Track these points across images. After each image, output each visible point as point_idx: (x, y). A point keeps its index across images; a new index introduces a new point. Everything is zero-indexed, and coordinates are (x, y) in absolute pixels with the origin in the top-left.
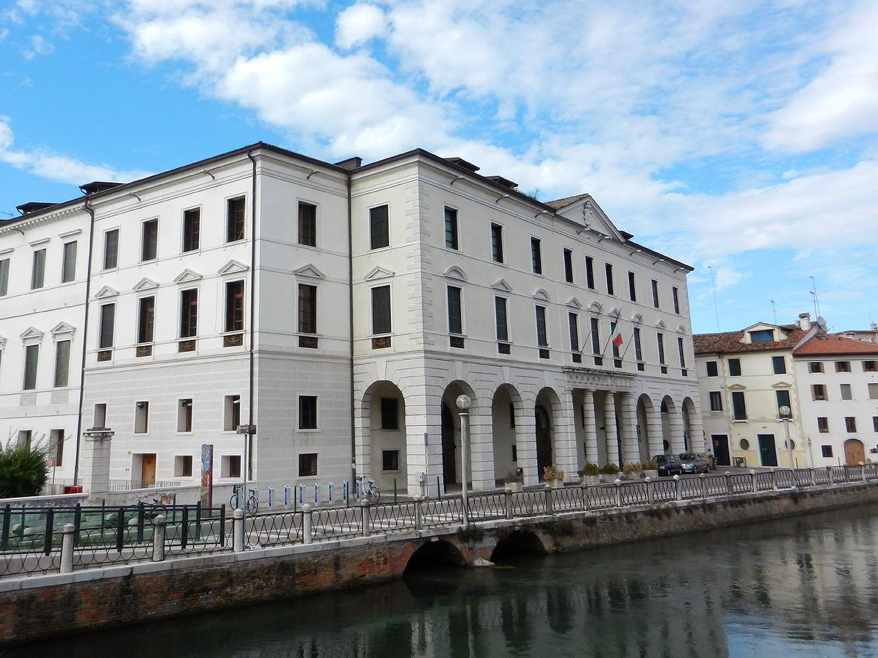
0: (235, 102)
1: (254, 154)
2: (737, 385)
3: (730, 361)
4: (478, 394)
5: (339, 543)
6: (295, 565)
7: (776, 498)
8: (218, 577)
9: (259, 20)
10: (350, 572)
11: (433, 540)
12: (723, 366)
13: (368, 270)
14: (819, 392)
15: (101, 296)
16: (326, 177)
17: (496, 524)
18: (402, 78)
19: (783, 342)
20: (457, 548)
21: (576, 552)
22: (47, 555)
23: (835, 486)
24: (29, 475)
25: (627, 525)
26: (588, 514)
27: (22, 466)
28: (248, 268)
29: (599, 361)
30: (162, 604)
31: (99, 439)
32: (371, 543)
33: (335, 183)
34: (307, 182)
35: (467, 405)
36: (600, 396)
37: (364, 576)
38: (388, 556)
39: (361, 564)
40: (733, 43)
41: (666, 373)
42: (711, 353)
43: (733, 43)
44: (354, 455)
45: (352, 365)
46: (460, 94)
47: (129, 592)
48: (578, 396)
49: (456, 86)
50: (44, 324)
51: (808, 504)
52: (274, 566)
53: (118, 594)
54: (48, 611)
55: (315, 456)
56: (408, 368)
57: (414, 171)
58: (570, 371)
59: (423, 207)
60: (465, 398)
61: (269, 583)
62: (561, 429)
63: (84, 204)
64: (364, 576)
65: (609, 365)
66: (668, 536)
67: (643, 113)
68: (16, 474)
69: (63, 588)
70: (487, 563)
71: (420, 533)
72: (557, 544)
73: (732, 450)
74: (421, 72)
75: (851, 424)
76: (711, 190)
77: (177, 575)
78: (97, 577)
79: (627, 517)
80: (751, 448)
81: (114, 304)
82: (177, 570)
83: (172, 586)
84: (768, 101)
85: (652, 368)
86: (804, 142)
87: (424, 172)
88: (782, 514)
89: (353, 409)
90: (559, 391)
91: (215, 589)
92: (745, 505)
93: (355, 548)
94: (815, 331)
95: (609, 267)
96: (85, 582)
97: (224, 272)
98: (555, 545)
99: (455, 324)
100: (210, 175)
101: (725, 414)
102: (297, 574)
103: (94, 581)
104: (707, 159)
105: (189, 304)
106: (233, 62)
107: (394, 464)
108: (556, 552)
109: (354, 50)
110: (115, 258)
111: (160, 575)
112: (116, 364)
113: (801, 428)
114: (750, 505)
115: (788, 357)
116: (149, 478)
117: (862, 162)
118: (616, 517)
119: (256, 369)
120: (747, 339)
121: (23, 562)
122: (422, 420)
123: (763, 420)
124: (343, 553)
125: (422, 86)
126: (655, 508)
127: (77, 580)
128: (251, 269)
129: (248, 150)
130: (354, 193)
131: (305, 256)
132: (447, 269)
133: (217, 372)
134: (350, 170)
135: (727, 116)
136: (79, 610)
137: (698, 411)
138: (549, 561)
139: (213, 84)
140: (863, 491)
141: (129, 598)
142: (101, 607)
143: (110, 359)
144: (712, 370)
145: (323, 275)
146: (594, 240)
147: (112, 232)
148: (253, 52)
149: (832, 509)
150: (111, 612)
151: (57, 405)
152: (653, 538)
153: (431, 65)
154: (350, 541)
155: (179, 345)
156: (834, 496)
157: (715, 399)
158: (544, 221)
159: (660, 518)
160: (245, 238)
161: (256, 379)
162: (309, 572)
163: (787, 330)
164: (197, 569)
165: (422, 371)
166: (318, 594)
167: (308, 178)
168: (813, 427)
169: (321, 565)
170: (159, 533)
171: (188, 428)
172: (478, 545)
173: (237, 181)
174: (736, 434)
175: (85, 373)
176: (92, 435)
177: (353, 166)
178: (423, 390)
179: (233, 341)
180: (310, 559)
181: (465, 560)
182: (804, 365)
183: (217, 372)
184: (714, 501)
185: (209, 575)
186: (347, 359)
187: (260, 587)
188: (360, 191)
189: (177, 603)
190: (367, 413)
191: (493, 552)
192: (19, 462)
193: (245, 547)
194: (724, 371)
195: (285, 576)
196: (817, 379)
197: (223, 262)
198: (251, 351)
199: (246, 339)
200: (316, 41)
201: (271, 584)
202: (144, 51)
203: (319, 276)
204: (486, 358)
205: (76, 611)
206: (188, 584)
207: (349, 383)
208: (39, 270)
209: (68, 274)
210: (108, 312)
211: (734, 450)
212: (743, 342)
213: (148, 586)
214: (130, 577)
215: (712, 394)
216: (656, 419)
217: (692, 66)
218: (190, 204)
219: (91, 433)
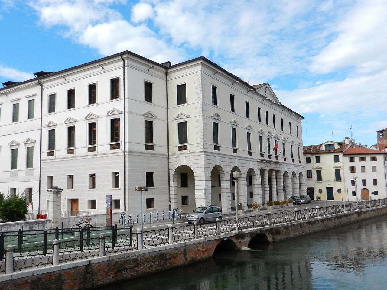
0: (88, 46)
1: (124, 57)
2: (318, 167)
3: (316, 157)
4: (242, 172)
5: (186, 243)
6: (166, 254)
7: (352, 214)
8: (131, 263)
9: (97, 8)
10: (191, 256)
11: (225, 239)
12: (313, 159)
13: (176, 115)
14: (352, 169)
15: (48, 126)
16: (156, 69)
17: (250, 230)
18: (161, 37)
19: (338, 149)
20: (234, 242)
21: (281, 241)
22: (45, 256)
23: (371, 208)
24: (19, 209)
25: (300, 228)
26: (286, 224)
27: (16, 205)
28: (122, 112)
29: (277, 158)
30: (105, 278)
31: (55, 193)
32: (199, 242)
33: (160, 73)
34: (148, 72)
35: (238, 176)
36: (270, 171)
37: (197, 257)
38: (206, 248)
39: (195, 252)
40: (299, 26)
41: (286, 161)
42: (308, 154)
43: (299, 26)
44: (170, 199)
45: (168, 158)
46: (186, 45)
47: (89, 273)
48: (262, 171)
49: (184, 41)
50: (20, 139)
51: (363, 216)
52: (157, 256)
53: (83, 274)
54: (48, 285)
55: (153, 199)
56: (195, 158)
57: (199, 67)
58: (260, 161)
59: (203, 84)
60: (237, 173)
61: (155, 264)
62: (256, 186)
63: (37, 81)
64: (197, 257)
65: (273, 159)
66: (315, 233)
67: (262, 56)
68: (13, 209)
69: (55, 273)
70: (248, 249)
71: (220, 236)
72: (274, 238)
73: (315, 194)
74: (169, 35)
75: (364, 182)
76: (287, 89)
77: (112, 263)
78: (73, 266)
79: (300, 225)
80: (323, 193)
81: (55, 129)
82: (112, 260)
83: (110, 268)
84: (312, 51)
85: (289, 161)
86: (326, 70)
87: (203, 67)
88: (354, 221)
89: (169, 178)
90: (255, 170)
91: (130, 268)
92: (341, 218)
93: (193, 245)
94: (351, 145)
95: (274, 116)
96: (66, 269)
97: (110, 114)
98: (273, 239)
99: (216, 140)
100: (101, 67)
101: (313, 179)
102: (168, 259)
103: (71, 268)
104: (287, 76)
105: (92, 129)
106: (86, 27)
107: (186, 202)
108: (273, 242)
109: (140, 24)
110: (54, 108)
111: (104, 264)
112: (57, 157)
113: (344, 184)
114: (343, 218)
115: (341, 155)
116: (75, 210)
117: (347, 78)
118: (296, 225)
119: (127, 160)
120: (323, 148)
121: (33, 260)
122: (203, 183)
123: (329, 181)
124: (187, 247)
125: (169, 41)
126: (310, 220)
127: (63, 268)
128: (123, 112)
129: (121, 54)
130: (169, 78)
131: (147, 107)
132: (213, 114)
133: (107, 161)
134: (167, 67)
135: (296, 58)
136: (65, 284)
137: (304, 178)
138: (270, 247)
139: (78, 37)
140: (380, 210)
141: (89, 276)
142: (75, 281)
143: (54, 155)
144: (308, 161)
145: (156, 117)
146: (269, 104)
147: (52, 95)
148: (95, 23)
149: (371, 218)
150: (80, 283)
151: (28, 176)
152: (309, 234)
153: (173, 31)
154: (190, 242)
155: (67, 151)
156: (371, 213)
157: (309, 173)
158: (250, 94)
159: (312, 225)
160: (120, 98)
161: (127, 164)
162: (173, 258)
163: (340, 144)
164: (122, 259)
165: (203, 161)
166: (177, 268)
167: (149, 70)
168: (349, 185)
169: (178, 254)
170: (102, 242)
171: (94, 187)
172: (243, 241)
173: (116, 70)
174: (317, 187)
175: (42, 162)
176: (52, 191)
177: (167, 66)
178: (203, 170)
179: (115, 146)
180: (173, 251)
181: (237, 247)
182: (347, 159)
183: (107, 161)
184: (331, 217)
185: (127, 262)
186: (166, 155)
187: (151, 266)
188: (172, 77)
189: (113, 276)
190: (175, 180)
191: (249, 243)
192: (14, 203)
193: (143, 247)
194: (313, 161)
195: (162, 260)
196: (352, 164)
197: (109, 110)
198: (124, 151)
199: (122, 146)
200: (122, 19)
201: (156, 264)
202: (45, 20)
203: (154, 117)
204: (228, 155)
205: (63, 284)
206: (117, 266)
207: (167, 166)
208: (16, 112)
209: (30, 115)
210: (51, 133)
211: (316, 194)
212: (322, 149)
213: (99, 269)
214: (89, 265)
215: (308, 171)
216: (289, 182)
217: (282, 35)
218: (91, 81)
219: (52, 190)
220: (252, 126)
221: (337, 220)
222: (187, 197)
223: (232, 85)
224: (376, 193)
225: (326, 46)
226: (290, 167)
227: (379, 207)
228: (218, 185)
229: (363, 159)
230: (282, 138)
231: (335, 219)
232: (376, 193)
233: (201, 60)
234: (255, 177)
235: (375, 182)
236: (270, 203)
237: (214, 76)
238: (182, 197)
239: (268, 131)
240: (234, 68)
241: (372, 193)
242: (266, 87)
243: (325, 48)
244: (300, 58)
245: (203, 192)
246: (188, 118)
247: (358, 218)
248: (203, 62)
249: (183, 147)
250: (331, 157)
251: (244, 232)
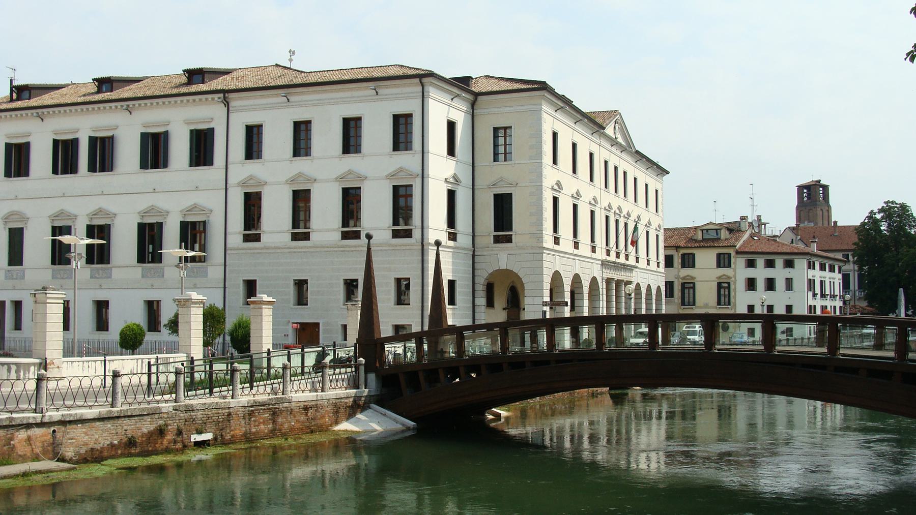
48: (609, 281)
58: (604, 264)
65: (622, 260)
95: (555, 135)
196: (751, 273)
199: (417, 234)
218: (351, 112)
223: (573, 125)
241: (783, 332)
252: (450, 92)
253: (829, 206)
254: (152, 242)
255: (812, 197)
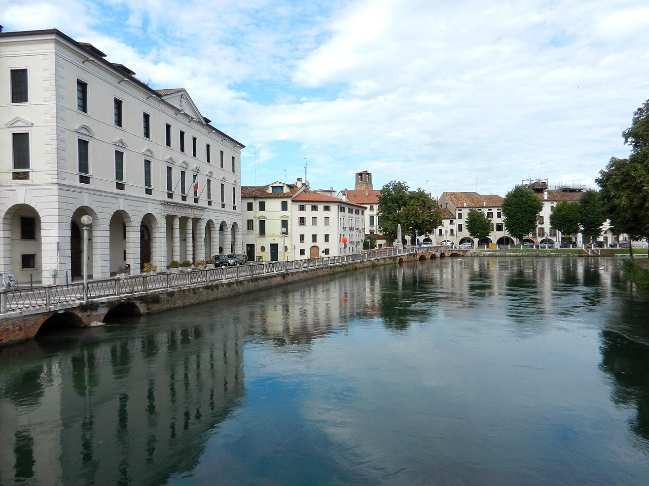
3: (283, 202)
4: (99, 216)
7: (275, 276)
12: (256, 205)
14: (302, 221)
23: (303, 269)
26: (170, 290)
36: (183, 220)
42: (250, 197)
48: (170, 219)
51: (289, 279)
58: (165, 204)
59: (58, 77)
60: (88, 218)
62: (157, 240)
66: (216, 300)
67: (227, 44)
71: (50, 308)
72: (149, 309)
75: (315, 238)
79: (193, 291)
80: (266, 251)
85: (217, 204)
87: (59, 48)
88: (277, 285)
94: (304, 188)
95: (194, 140)
98: (147, 310)
101: (255, 232)
108: (148, 314)
112: (34, 182)
113: (291, 240)
114: (261, 280)
115: (289, 201)
117: (339, 99)
120: (270, 191)
122: (56, 233)
123: (273, 235)
132: (78, 126)
138: (142, 319)
144: (250, 207)
146: (186, 120)
149: (300, 281)
152: (207, 302)
157: (250, 222)
159: (213, 290)
163: (290, 187)
165: (56, 199)
172: (94, 313)
182: (296, 206)
194: (256, 208)
196: (302, 214)
211: (257, 252)
216: (216, 234)
220: (154, 151)
221: (251, 283)
222: (34, 255)
224: (327, 251)
225: (315, 48)
226: (218, 214)
227: (314, 268)
228: (123, 238)
229: (314, 208)
230: (207, 173)
231: (248, 283)
232: (327, 251)
233: (55, 35)
234: (156, 226)
235: (327, 238)
236: (173, 264)
237: (82, 65)
238: (23, 255)
239: (182, 161)
240: (184, 55)
241: (323, 252)
242: (182, 95)
243: (315, 50)
244: (282, 58)
245: (55, 246)
246: (30, 127)
247: (283, 282)
248: (57, 38)
249: (21, 174)
250: (278, 203)
251: (97, 301)
252: (117, 77)
253: (371, 184)
254: (168, 203)
255: (364, 177)
